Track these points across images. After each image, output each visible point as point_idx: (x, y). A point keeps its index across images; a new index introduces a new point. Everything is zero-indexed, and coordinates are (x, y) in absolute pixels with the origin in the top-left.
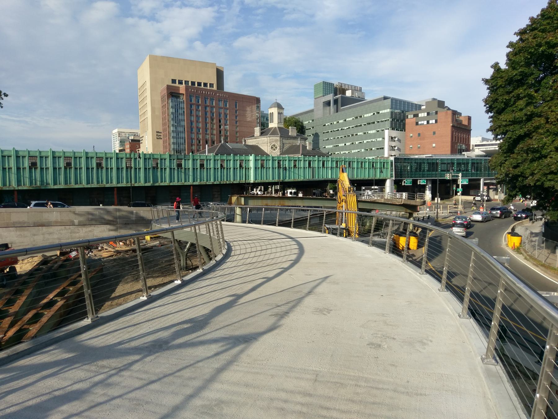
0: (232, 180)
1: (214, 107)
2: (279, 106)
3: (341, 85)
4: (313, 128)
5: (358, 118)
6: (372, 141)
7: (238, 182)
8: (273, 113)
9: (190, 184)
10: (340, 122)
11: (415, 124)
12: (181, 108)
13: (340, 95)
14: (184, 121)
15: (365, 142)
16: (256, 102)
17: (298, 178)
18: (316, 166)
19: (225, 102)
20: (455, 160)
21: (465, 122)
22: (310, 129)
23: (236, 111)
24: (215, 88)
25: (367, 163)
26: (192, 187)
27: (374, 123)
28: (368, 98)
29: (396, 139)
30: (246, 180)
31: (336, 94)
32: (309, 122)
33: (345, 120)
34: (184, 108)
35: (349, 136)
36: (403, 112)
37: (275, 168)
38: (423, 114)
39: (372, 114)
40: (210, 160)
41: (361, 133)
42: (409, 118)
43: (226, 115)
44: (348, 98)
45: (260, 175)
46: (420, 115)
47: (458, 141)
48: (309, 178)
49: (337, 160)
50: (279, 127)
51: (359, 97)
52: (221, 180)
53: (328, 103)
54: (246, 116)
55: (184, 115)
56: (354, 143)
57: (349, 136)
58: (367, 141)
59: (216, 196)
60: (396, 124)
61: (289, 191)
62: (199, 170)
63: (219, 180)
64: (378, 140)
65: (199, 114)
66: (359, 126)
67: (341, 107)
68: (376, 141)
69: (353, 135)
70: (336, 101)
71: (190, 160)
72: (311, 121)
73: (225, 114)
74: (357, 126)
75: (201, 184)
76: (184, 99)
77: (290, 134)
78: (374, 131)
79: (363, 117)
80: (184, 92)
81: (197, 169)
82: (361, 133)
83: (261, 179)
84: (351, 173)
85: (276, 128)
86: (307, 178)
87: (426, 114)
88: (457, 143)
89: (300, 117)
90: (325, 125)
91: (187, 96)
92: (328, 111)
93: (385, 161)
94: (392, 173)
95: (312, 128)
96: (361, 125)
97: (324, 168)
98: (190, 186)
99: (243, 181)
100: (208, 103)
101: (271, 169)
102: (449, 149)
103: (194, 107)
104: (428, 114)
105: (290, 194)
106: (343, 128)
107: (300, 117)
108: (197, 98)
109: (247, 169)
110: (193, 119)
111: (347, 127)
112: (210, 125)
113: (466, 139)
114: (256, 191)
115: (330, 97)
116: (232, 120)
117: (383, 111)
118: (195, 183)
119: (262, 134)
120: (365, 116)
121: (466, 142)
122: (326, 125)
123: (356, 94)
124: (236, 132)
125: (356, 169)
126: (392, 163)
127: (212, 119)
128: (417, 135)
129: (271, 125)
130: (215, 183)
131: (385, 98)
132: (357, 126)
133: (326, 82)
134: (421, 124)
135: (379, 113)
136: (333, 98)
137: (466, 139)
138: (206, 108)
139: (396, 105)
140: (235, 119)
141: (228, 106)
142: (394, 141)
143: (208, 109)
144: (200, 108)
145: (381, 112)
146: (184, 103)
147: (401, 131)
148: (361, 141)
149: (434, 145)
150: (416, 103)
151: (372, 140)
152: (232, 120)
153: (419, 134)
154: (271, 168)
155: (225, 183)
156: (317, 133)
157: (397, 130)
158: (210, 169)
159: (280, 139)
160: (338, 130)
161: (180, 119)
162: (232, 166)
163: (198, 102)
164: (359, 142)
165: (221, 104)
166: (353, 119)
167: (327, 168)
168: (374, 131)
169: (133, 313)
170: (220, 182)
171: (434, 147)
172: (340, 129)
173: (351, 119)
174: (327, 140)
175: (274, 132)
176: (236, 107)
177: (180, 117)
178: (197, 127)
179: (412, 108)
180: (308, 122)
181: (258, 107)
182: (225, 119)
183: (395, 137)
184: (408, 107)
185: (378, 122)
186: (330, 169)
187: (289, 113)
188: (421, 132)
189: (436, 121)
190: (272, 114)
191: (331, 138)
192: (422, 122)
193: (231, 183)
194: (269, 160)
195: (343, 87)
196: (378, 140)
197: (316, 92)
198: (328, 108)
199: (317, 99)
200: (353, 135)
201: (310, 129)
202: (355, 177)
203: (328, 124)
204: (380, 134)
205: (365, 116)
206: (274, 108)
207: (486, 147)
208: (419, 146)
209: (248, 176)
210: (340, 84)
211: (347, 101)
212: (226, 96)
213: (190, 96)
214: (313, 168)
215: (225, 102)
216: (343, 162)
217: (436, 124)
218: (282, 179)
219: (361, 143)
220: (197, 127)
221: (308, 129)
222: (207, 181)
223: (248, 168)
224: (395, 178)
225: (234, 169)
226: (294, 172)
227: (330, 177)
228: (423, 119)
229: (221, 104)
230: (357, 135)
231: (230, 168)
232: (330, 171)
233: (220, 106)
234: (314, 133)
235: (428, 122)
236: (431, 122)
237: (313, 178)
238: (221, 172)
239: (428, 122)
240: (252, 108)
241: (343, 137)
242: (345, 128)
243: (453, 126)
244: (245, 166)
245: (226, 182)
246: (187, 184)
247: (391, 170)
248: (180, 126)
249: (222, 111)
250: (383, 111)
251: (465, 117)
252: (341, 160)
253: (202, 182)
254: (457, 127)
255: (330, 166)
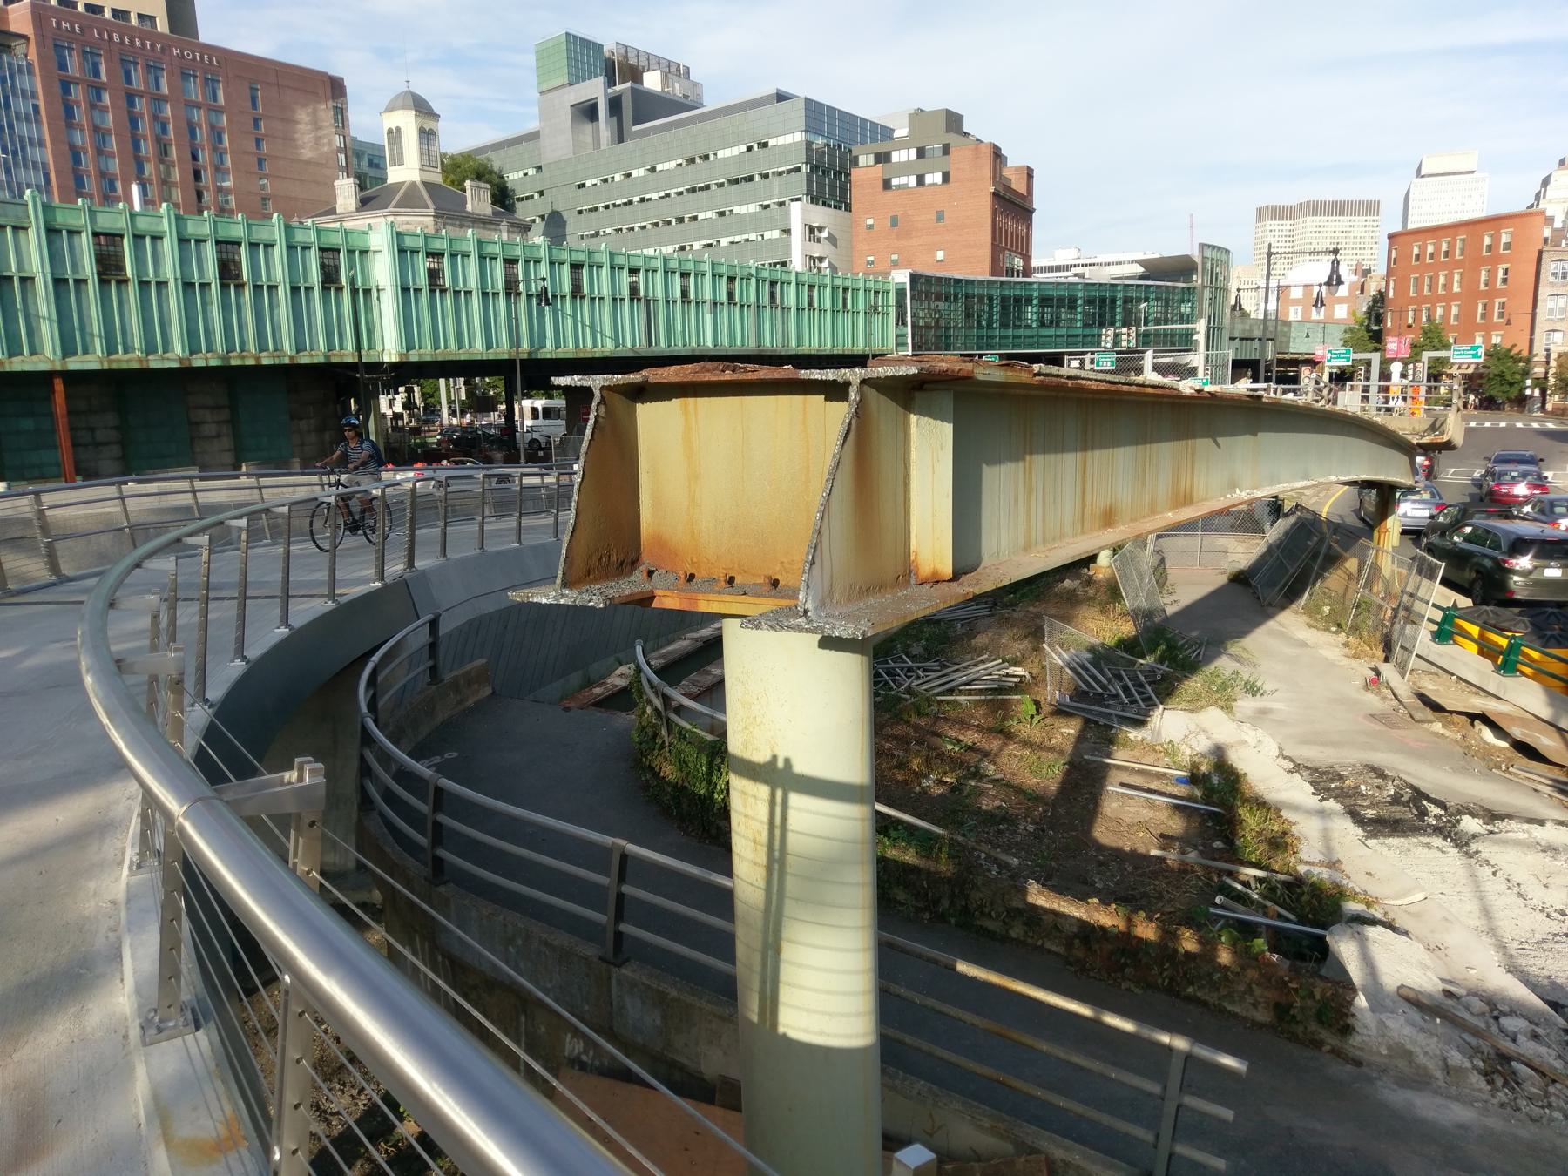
0: (288, 347)
1: (165, 99)
2: (422, 108)
3: (626, 51)
4: (541, 193)
5: (698, 160)
6: (747, 240)
7: (322, 360)
8: (398, 130)
9: (44, 367)
10: (635, 173)
11: (880, 184)
12: (23, 91)
13: (628, 85)
14: (42, 144)
15: (724, 242)
16: (329, 93)
17: (595, 346)
18: (660, 294)
19: (210, 83)
20: (1080, 287)
21: (1019, 186)
22: (532, 197)
23: (256, 121)
24: (162, 26)
25: (828, 290)
26: (59, 385)
27: (750, 179)
28: (710, 104)
29: (825, 234)
30: (359, 347)
31: (611, 82)
32: (526, 174)
33: (653, 170)
34: (34, 95)
35: (669, 223)
36: (840, 146)
37: (495, 294)
38: (904, 159)
39: (743, 148)
40: (157, 238)
41: (710, 214)
42: (860, 165)
43: (217, 134)
44: (650, 96)
45: (450, 320)
46: (896, 157)
47: (1006, 244)
48: (634, 345)
49: (732, 273)
50: (426, 184)
51: (686, 97)
52: (230, 349)
53: (588, 112)
54: (294, 140)
55: (38, 121)
56: (688, 248)
57: (669, 223)
58: (731, 239)
59: (209, 429)
60: (821, 185)
61: (527, 403)
62: (92, 287)
63: (219, 346)
64: (767, 235)
65: (103, 121)
66: (701, 189)
67: (635, 124)
68: (760, 239)
69: (681, 220)
70: (615, 105)
71: (32, 233)
72: (531, 172)
73: (212, 127)
74: (693, 190)
75: (115, 366)
76: (33, 56)
77: (469, 207)
78: (753, 208)
79: (712, 157)
80: (28, 30)
81: (80, 283)
82: (710, 214)
83: (437, 347)
84: (779, 325)
85: (414, 184)
86: (629, 345)
87: (913, 154)
88: (1004, 249)
89: (492, 155)
90: (584, 185)
91: (41, 44)
92: (589, 139)
93: (880, 286)
94: (901, 329)
95: (536, 196)
96: (707, 187)
97: (689, 302)
98: (47, 377)
99: (346, 353)
100: (138, 80)
101: (476, 299)
102: (986, 265)
103: (77, 93)
104: (921, 153)
105: (1499, 317)
106: (647, 196)
107: (492, 155)
108: (90, 57)
109: (363, 294)
110: (81, 138)
111: (662, 194)
112: (157, 169)
113: (1022, 238)
114: (391, 407)
115: (595, 89)
116: (245, 152)
117: (781, 140)
118: (74, 364)
119: (365, 203)
120: (720, 154)
121: (1022, 250)
122: (588, 183)
123: (677, 85)
124: (264, 199)
125: (793, 311)
126: (900, 293)
127: (163, 150)
128: (888, 223)
129: (394, 175)
130: (198, 362)
131: (781, 97)
132: (693, 190)
133: (575, 37)
134: (899, 187)
135: (765, 145)
136: (605, 91)
137: (1022, 238)
138: (130, 98)
139: (820, 121)
140: (254, 149)
141: (221, 100)
142: (819, 241)
143: (141, 105)
144: (106, 98)
145: (772, 142)
146: (31, 72)
147: (835, 207)
148: (709, 242)
149: (940, 255)
150: (876, 121)
151: (746, 236)
152: (245, 152)
153: (894, 222)
154: (475, 294)
155: (251, 362)
156: (558, 212)
157: (824, 204)
158: (162, 285)
159: (436, 223)
160: (630, 202)
161: (21, 139)
162: (280, 275)
163: (97, 74)
164: (704, 242)
165: (195, 90)
166: (681, 165)
167: (697, 303)
168: (753, 208)
169: (160, 476)
170: (223, 358)
171: (941, 261)
172: (636, 199)
173: (673, 164)
174: (592, 236)
175: (410, 198)
176: (254, 106)
177: (23, 129)
178: (103, 175)
179: (864, 136)
180: (521, 174)
181: (340, 113)
182: (215, 149)
183: (821, 229)
184: (853, 132)
185: (766, 176)
186: (708, 306)
187: (456, 139)
188: (899, 212)
189: (946, 178)
190: (394, 134)
191: (608, 231)
192: (903, 180)
193: (287, 361)
194: (466, 256)
195: (633, 61)
196: (767, 235)
197: (543, 69)
198: (588, 127)
199: (549, 95)
200: (681, 220)
201: (532, 197)
202: (793, 343)
203: (594, 181)
204: (775, 212)
205: (720, 154)
206: (401, 112)
207: (1058, 274)
208: (895, 257)
209: (370, 332)
210: (622, 51)
211: (649, 107)
212: (210, 60)
213: (58, 48)
214: (648, 301)
215: (210, 83)
216: (753, 280)
217: (946, 186)
218: (525, 345)
219: (710, 245)
220: (103, 175)
221: (522, 199)
222: (150, 348)
223: (367, 292)
224: (913, 350)
225: (295, 290)
226: (574, 316)
227: (710, 343)
228: (905, 169)
229: (195, 90)
230: (695, 218)
231: (273, 288)
232: (709, 317)
233: (190, 96)
234: (547, 212)
235: (921, 181)
236: (929, 179)
237: (650, 344)
238: (226, 306)
239: (921, 181)
240: (315, 112)
241: (649, 227)
242: (655, 196)
243: (995, 195)
244: (352, 281)
245: (258, 359)
246: (27, 368)
247: (901, 320)
248: (26, 166)
249: (198, 116)
250: (781, 140)
251: (1018, 169)
252: (745, 273)
253: (120, 354)
254: (1003, 198)
255: (708, 296)
